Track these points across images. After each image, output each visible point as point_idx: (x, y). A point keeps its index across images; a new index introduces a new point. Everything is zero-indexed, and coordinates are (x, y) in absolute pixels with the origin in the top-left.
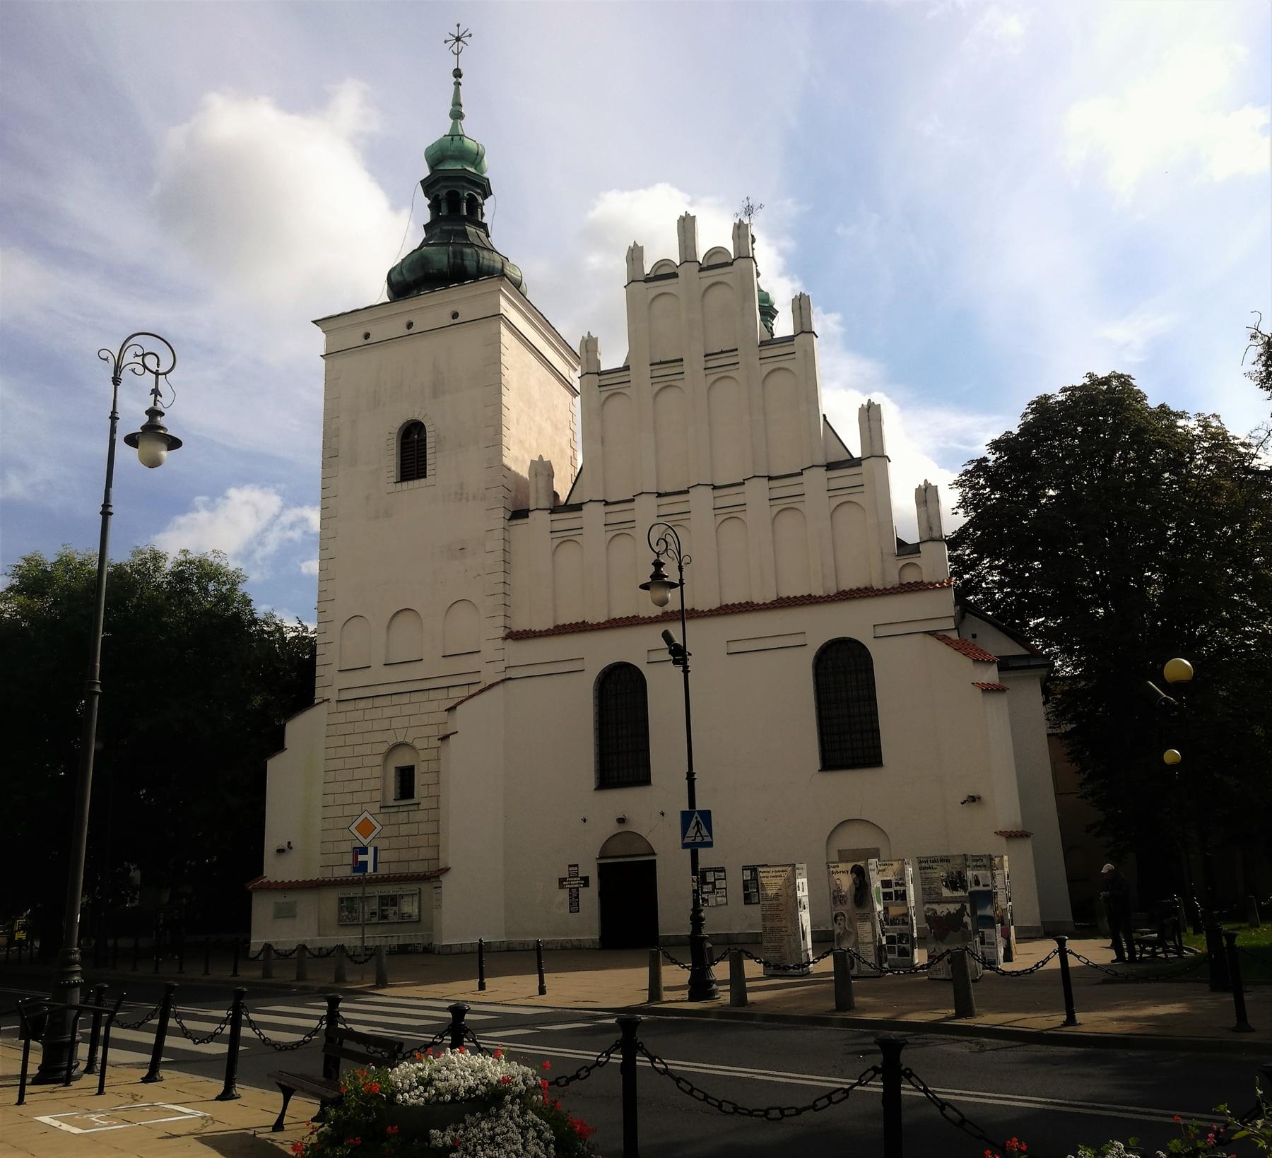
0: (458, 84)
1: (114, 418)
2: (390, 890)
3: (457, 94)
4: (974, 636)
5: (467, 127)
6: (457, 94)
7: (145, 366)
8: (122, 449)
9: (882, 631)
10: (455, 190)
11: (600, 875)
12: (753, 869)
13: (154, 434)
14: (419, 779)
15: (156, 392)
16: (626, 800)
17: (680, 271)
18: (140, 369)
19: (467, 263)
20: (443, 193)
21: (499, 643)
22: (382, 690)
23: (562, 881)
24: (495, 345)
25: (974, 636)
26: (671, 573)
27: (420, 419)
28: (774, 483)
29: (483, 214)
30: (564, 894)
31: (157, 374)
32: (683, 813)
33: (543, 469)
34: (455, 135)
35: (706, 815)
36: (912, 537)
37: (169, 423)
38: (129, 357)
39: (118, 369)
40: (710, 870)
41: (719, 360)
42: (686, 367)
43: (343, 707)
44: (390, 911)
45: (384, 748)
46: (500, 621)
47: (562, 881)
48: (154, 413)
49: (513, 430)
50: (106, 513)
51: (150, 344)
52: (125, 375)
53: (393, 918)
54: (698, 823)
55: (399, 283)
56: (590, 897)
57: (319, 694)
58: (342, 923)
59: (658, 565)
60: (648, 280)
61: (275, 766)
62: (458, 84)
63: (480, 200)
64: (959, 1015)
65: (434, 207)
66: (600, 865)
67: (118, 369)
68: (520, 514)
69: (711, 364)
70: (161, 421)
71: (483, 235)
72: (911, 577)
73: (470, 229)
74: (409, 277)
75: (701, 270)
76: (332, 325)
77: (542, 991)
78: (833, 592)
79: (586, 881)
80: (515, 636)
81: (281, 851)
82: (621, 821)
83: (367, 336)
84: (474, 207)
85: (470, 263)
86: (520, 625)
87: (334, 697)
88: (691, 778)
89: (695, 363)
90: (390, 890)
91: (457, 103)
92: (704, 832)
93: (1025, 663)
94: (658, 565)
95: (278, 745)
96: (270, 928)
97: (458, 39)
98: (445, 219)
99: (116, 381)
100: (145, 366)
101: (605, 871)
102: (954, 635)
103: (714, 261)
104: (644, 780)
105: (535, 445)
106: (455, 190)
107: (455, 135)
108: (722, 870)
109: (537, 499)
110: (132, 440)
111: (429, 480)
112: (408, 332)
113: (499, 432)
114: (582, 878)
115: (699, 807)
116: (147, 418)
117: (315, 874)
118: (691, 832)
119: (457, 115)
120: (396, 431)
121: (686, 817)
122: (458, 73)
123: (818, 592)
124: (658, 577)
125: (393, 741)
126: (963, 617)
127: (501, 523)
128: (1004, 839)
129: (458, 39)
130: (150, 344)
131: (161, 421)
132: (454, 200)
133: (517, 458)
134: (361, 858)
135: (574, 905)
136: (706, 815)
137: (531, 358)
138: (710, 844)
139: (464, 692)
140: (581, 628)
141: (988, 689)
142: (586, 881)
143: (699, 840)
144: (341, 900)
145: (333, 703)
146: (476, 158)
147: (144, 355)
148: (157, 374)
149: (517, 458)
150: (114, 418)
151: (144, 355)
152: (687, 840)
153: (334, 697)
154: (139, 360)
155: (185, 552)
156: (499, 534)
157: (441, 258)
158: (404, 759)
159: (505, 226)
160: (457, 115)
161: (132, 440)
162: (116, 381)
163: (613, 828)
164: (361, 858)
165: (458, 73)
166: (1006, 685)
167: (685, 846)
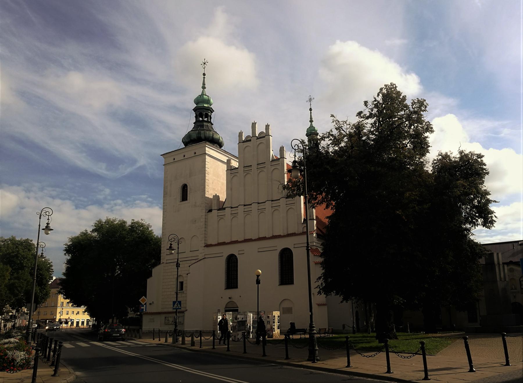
0: (204, 78)
1: (39, 226)
3: (204, 80)
6: (204, 80)
9: (296, 246)
13: (48, 228)
15: (48, 219)
16: (231, 292)
17: (252, 139)
19: (201, 136)
20: (198, 113)
21: (203, 248)
24: (204, 161)
26: (175, 246)
28: (273, 202)
33: (217, 197)
34: (203, 94)
37: (51, 226)
39: (40, 216)
41: (261, 165)
42: (252, 168)
43: (167, 265)
46: (203, 242)
48: (48, 224)
49: (210, 186)
51: (47, 210)
58: (166, 324)
60: (244, 142)
62: (204, 78)
63: (210, 114)
64: (192, 346)
67: (40, 216)
68: (210, 211)
69: (259, 167)
70: (50, 225)
76: (165, 156)
78: (286, 234)
80: (207, 246)
81: (150, 304)
82: (230, 298)
85: (202, 136)
86: (209, 243)
87: (165, 262)
89: (254, 167)
92: (179, 306)
94: (171, 244)
95: (150, 275)
96: (147, 325)
99: (40, 218)
103: (261, 136)
104: (237, 287)
105: (220, 189)
109: (215, 207)
111: (188, 201)
113: (205, 188)
115: (178, 300)
117: (160, 310)
118: (175, 306)
119: (204, 88)
121: (174, 303)
123: (282, 234)
124: (170, 247)
127: (204, 214)
129: (205, 64)
130: (47, 210)
131: (50, 225)
133: (210, 194)
136: (180, 302)
137: (219, 163)
139: (194, 261)
140: (224, 244)
144: (166, 318)
146: (208, 102)
149: (210, 194)
150: (39, 226)
153: (165, 262)
155: (133, 220)
156: (204, 217)
160: (204, 88)
162: (40, 218)
163: (229, 300)
165: (204, 74)
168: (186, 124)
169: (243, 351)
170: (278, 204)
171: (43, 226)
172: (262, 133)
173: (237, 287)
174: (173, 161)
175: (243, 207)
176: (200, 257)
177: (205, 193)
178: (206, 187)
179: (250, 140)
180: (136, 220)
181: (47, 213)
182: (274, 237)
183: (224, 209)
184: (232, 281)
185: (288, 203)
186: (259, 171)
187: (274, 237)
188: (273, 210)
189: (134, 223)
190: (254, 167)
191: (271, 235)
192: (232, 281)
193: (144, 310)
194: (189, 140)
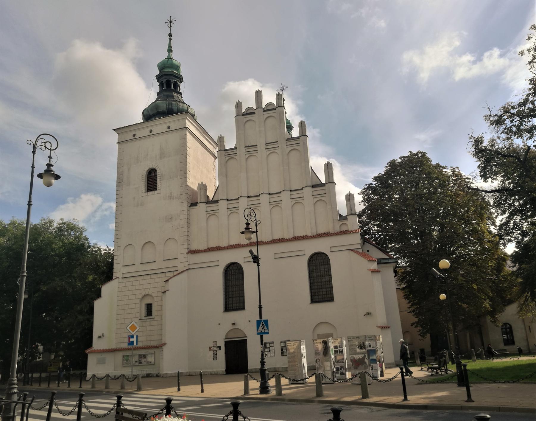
1: (33, 167)
2: (143, 352)
4: (368, 251)
5: (174, 55)
7: (45, 147)
8: (36, 179)
9: (333, 249)
10: (169, 80)
11: (226, 345)
12: (285, 342)
13: (49, 174)
14: (154, 309)
15: (50, 157)
16: (235, 316)
17: (256, 111)
18: (44, 148)
19: (173, 107)
20: (164, 81)
21: (186, 255)
22: (140, 274)
23: (210, 348)
25: (368, 251)
26: (252, 227)
27: (155, 167)
29: (180, 89)
30: (211, 353)
31: (51, 150)
32: (258, 321)
34: (169, 58)
35: (266, 322)
36: (344, 213)
37: (55, 169)
38: (39, 143)
39: (35, 148)
40: (268, 343)
42: (258, 148)
43: (124, 280)
44: (143, 360)
45: (140, 296)
46: (186, 246)
47: (210, 348)
48: (49, 165)
49: (191, 172)
50: (29, 205)
52: (38, 150)
53: (144, 363)
54: (263, 325)
55: (147, 115)
56: (222, 354)
57: (115, 275)
58: (124, 366)
59: (248, 224)
60: (243, 115)
61: (98, 304)
63: (179, 83)
65: (161, 86)
66: (226, 342)
67: (35, 148)
68: (194, 204)
71: (180, 97)
72: (344, 228)
73: (175, 94)
74: (151, 113)
75: (264, 111)
76: (121, 131)
77: (202, 391)
79: (220, 348)
80: (192, 252)
81: (99, 337)
82: (234, 324)
83: (134, 135)
84: (176, 86)
85: (175, 108)
86: (194, 247)
87: (121, 276)
88: (260, 307)
89: (261, 147)
90: (143, 352)
91: (170, 46)
92: (265, 328)
93: (387, 261)
94: (248, 224)
95: (98, 295)
97: (170, 22)
98: (165, 90)
99: (34, 152)
100: (45, 147)
101: (227, 344)
102: (360, 251)
103: (268, 108)
104: (243, 308)
106: (169, 80)
107: (169, 58)
108: (273, 343)
109: (200, 198)
110: (40, 176)
111: (158, 191)
112: (150, 134)
114: (218, 347)
116: (46, 167)
118: (261, 328)
119: (170, 51)
120: (145, 172)
121: (258, 323)
122: (170, 35)
123: (309, 234)
124: (247, 229)
125: (144, 294)
126: (364, 244)
127: (186, 208)
128: (380, 329)
129: (170, 22)
131: (52, 168)
132: (168, 83)
134: (131, 340)
135: (215, 357)
136: (266, 322)
138: (268, 333)
139: (172, 274)
140: (218, 249)
141: (374, 271)
142: (220, 348)
143: (263, 331)
145: (121, 279)
146: (177, 67)
147: (45, 143)
148: (51, 150)
150: (33, 167)
151: (45, 143)
152: (259, 332)
153: (120, 275)
154: (43, 144)
156: (185, 212)
157: (163, 106)
158: (148, 301)
159: (188, 93)
160: (170, 51)
161: (40, 176)
162: (34, 152)
164: (131, 340)
165: (170, 35)
166: (380, 270)
167: (258, 334)
168: (147, 94)
169: (466, 398)
170: (279, 199)
171: (41, 168)
172: (270, 104)
173: (243, 308)
174: (166, 130)
175: (246, 199)
176: (181, 268)
177: (186, 181)
178: (188, 172)
179: (254, 113)
180: (66, 221)
181: (48, 145)
182: (296, 239)
183: (217, 202)
184: (234, 299)
185: (315, 193)
186: (268, 153)
187: (296, 239)
188: (293, 203)
189: (65, 223)
190: (261, 147)
191: (291, 236)
192: (234, 299)
193: (135, 344)
194: (156, 112)
